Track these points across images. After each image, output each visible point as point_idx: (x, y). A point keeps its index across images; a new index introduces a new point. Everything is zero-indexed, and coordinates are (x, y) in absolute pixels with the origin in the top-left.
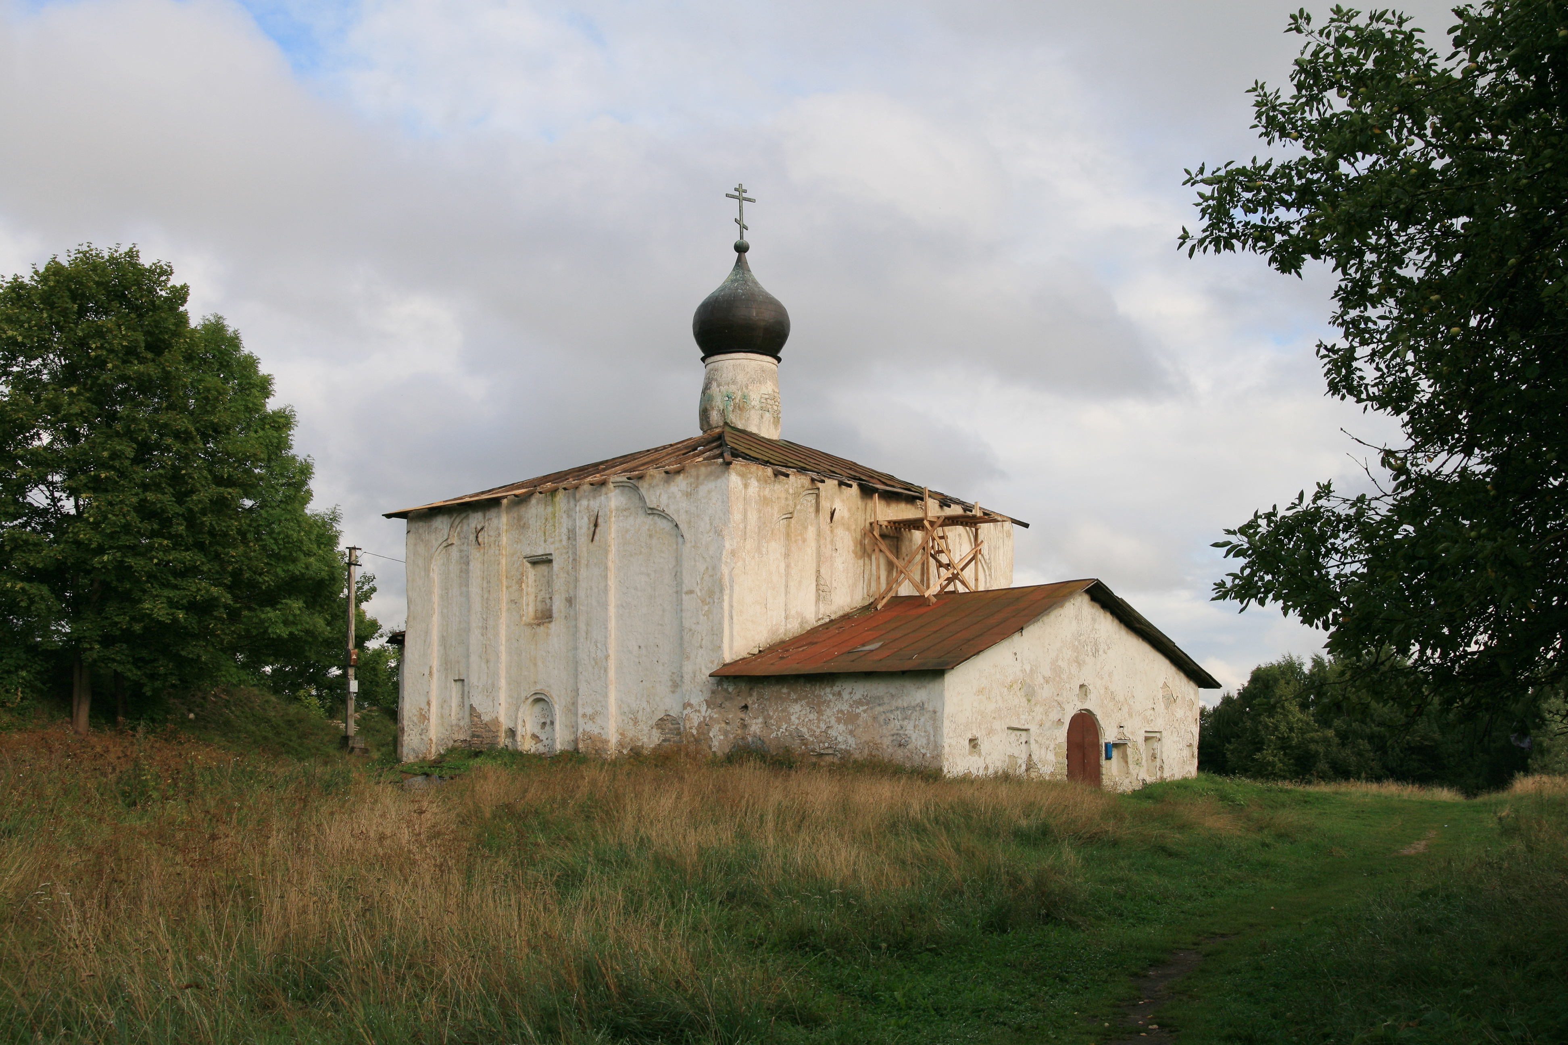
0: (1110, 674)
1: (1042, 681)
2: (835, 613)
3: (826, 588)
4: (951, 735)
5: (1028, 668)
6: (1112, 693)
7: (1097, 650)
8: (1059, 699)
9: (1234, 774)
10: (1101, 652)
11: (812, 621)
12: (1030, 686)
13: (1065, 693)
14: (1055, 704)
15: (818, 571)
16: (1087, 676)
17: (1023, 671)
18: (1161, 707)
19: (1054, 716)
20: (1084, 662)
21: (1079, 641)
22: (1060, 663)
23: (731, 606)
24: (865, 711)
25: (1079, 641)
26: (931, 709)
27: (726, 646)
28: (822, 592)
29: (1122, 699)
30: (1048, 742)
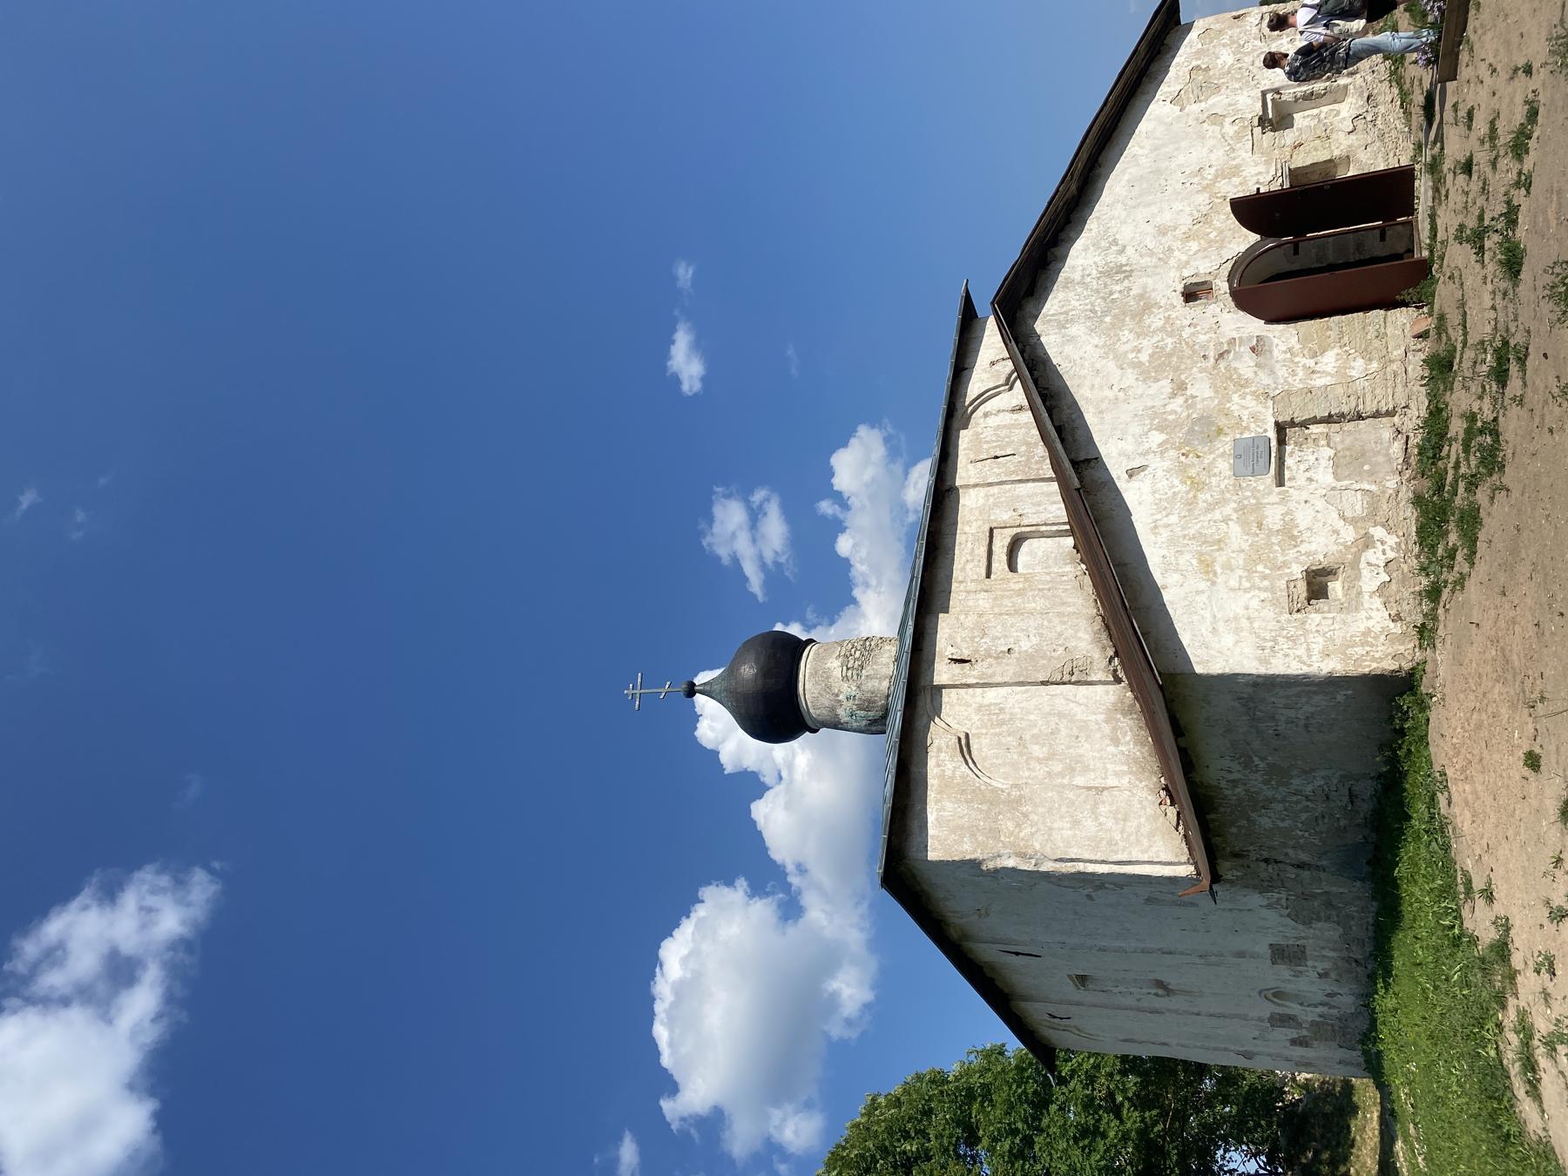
0: (1162, 231)
1: (1180, 400)
2: (1104, 648)
3: (1067, 669)
4: (1301, 651)
5: (1157, 438)
6: (1196, 222)
7: (1119, 269)
8: (1212, 354)
9: (1401, 733)
10: (1123, 259)
11: (1120, 694)
12: (1191, 431)
13: (1202, 338)
14: (1222, 365)
15: (1043, 683)
16: (1168, 287)
17: (1163, 449)
18: (1217, 102)
19: (1245, 364)
20: (1141, 296)
21: (1105, 313)
22: (1144, 357)
23: (1103, 862)
24: (1262, 759)
25: (1105, 313)
26: (1250, 690)
27: (1167, 871)
28: (1074, 677)
29: (1202, 199)
30: (1301, 374)
